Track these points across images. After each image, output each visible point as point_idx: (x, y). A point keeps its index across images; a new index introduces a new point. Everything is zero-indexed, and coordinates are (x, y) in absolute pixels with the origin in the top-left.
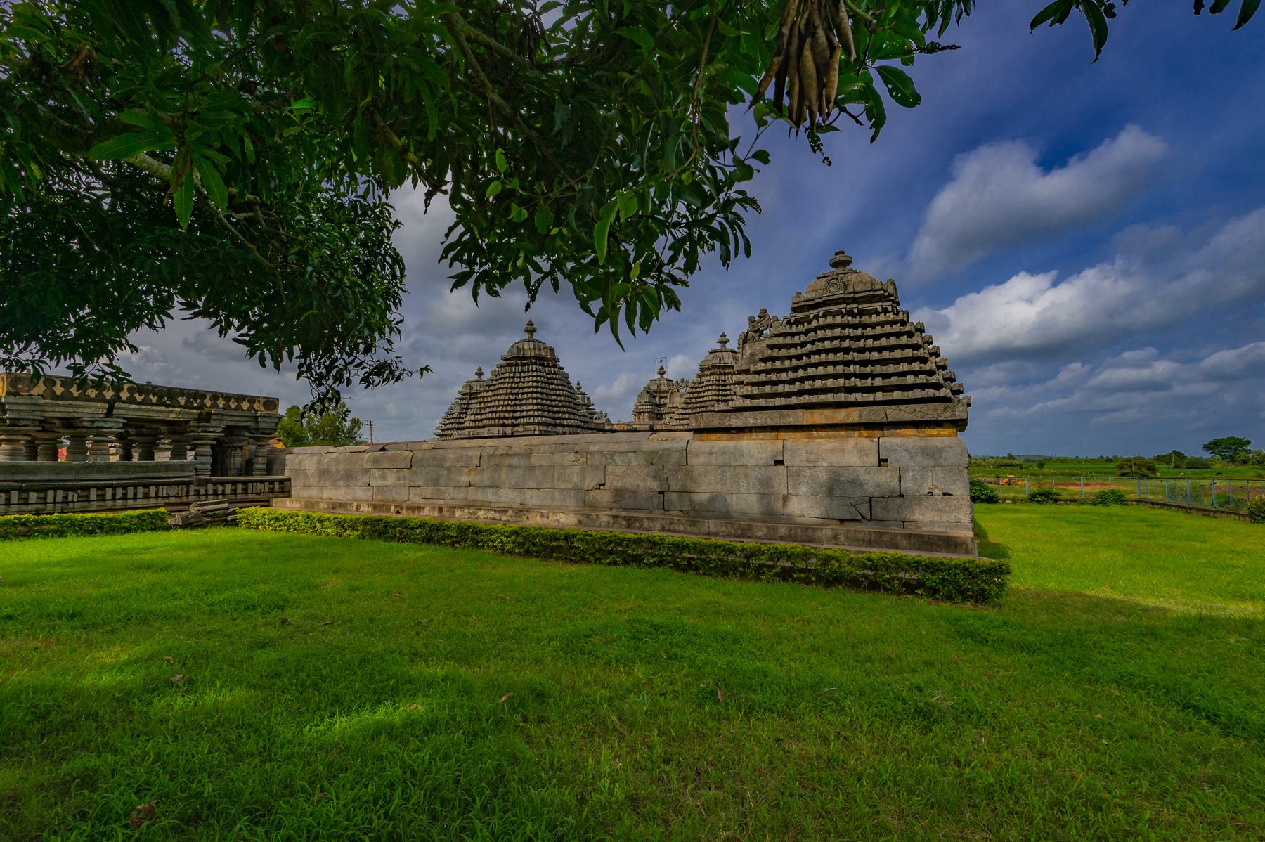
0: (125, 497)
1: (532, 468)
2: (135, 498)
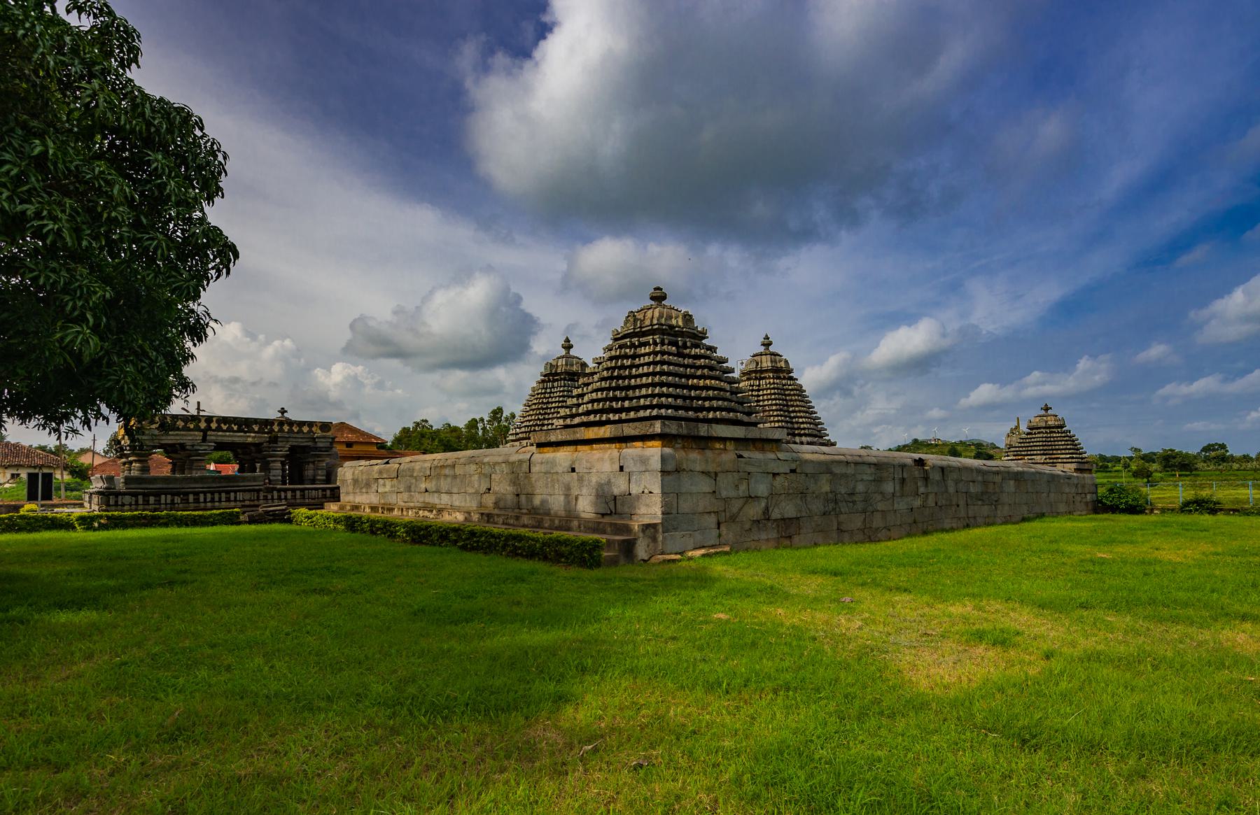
0: (213, 501)
1: (455, 477)
2: (220, 501)
